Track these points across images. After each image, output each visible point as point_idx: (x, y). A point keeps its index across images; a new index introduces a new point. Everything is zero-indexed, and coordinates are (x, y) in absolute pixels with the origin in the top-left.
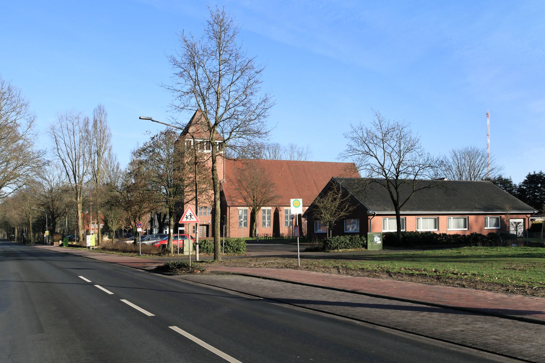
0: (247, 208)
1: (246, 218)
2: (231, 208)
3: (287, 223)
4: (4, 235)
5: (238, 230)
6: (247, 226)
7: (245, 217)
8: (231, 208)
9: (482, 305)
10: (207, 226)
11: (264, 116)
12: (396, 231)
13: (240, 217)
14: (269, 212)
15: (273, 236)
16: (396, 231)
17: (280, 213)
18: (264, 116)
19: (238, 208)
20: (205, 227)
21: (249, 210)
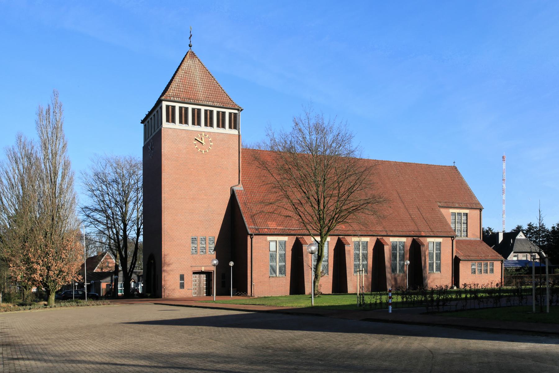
0: (286, 238)
1: (283, 258)
2: (255, 238)
3: (357, 266)
4: (536, 227)
5: (268, 282)
6: (285, 273)
7: (281, 255)
8: (255, 238)
9: (260, 331)
10: (208, 274)
11: (131, 161)
12: (205, 275)
13: (273, 257)
14: (366, 245)
15: (101, 282)
16: (205, 275)
17: (347, 248)
18: (131, 161)
19: (269, 238)
20: (204, 277)
21: (289, 241)
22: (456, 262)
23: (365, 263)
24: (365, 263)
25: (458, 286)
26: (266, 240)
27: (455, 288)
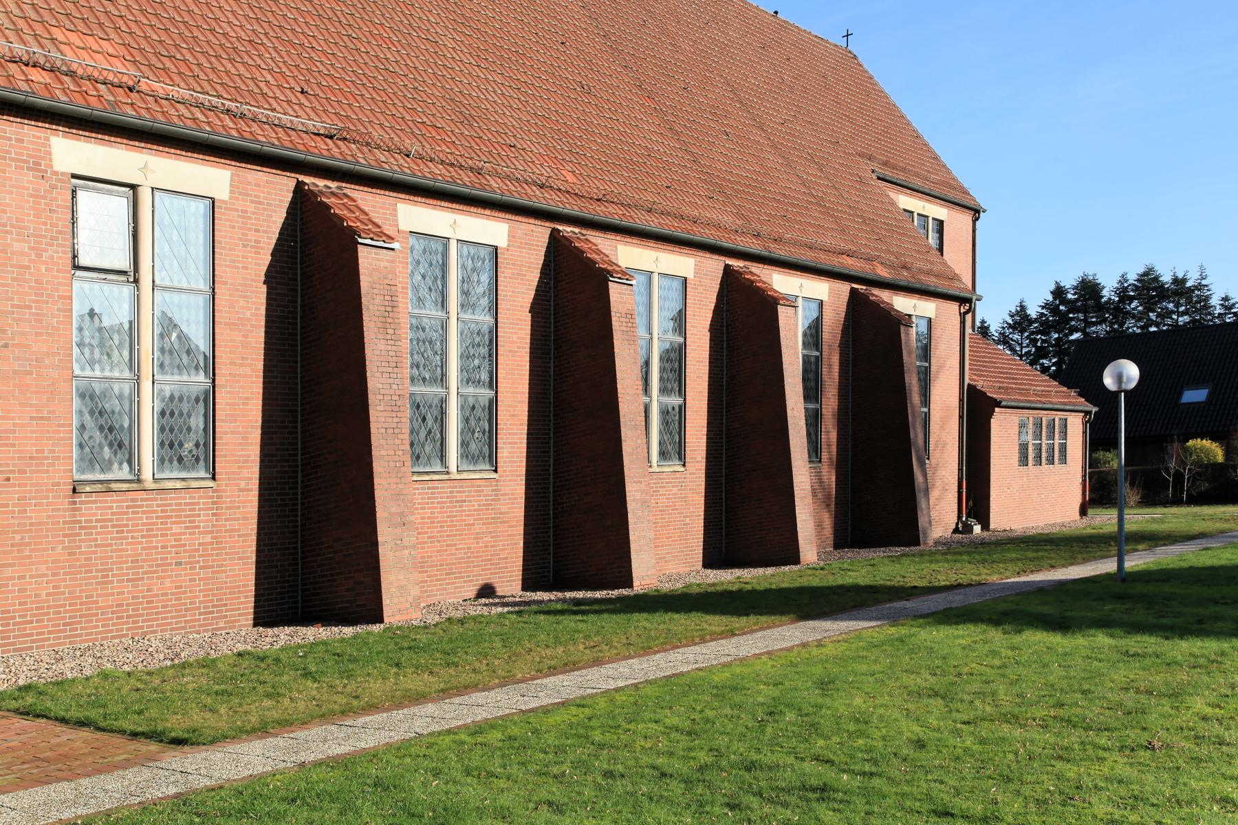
16: (1116, 529)
22: (977, 410)
23: (675, 400)
24: (675, 400)
25: (986, 526)
26: (39, 165)
27: (977, 529)
